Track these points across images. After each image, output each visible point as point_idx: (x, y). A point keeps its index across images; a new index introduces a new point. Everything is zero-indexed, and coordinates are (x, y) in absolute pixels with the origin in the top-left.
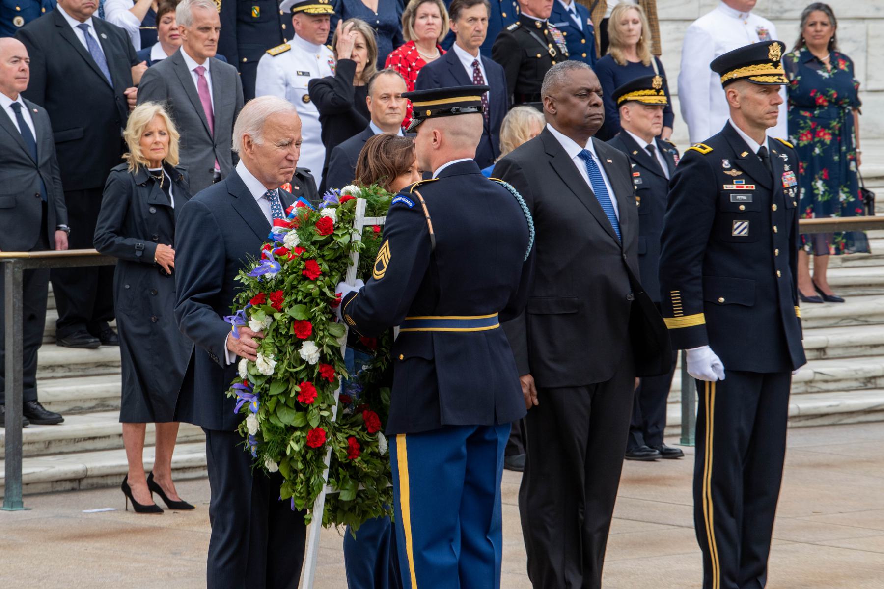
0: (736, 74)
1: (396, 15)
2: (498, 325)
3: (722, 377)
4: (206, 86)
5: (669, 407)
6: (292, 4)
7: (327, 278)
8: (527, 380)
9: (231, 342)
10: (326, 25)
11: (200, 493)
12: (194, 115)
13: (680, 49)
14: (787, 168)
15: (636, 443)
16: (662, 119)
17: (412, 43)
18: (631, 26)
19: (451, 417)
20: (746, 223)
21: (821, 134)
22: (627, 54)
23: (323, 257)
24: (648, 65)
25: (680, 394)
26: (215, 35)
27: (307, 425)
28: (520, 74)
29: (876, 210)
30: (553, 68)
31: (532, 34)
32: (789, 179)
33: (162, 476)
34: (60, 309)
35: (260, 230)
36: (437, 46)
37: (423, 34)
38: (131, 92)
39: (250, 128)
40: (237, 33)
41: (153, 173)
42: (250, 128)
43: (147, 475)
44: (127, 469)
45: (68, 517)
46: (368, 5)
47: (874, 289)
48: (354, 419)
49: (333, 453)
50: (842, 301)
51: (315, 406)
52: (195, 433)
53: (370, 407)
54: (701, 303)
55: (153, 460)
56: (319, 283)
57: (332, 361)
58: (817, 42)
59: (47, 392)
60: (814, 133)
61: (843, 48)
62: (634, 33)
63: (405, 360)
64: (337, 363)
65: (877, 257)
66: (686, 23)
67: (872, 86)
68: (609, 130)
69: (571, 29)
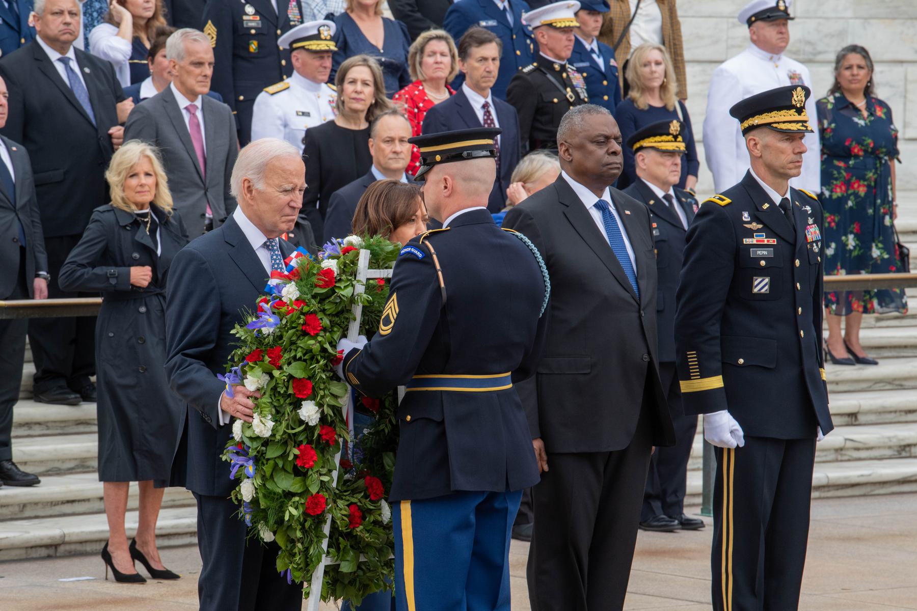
0: (757, 120)
1: (403, 53)
2: (511, 385)
3: (742, 444)
4: (198, 125)
5: (689, 475)
6: (291, 40)
7: (328, 334)
8: (537, 444)
9: (225, 402)
10: (328, 63)
11: (189, 564)
12: (185, 155)
13: (706, 92)
14: (810, 221)
15: (654, 513)
16: (680, 166)
17: (419, 83)
18: (654, 67)
19: (462, 482)
20: (767, 280)
21: (856, 186)
22: (649, 98)
23: (324, 311)
24: (671, 109)
25: (701, 461)
26: (209, 71)
27: (307, 491)
28: (535, 119)
29: (911, 266)
30: (570, 111)
31: (549, 76)
32: (813, 232)
33: (145, 543)
34: (37, 361)
35: (257, 279)
36: (446, 86)
37: (430, 73)
38: (116, 131)
39: (250, 172)
40: (234, 69)
41: (138, 215)
42: (250, 172)
43: (130, 542)
44: (107, 535)
45: (42, 586)
46: (373, 42)
47: (910, 351)
48: (355, 485)
49: (333, 522)
50: (876, 363)
51: (315, 470)
52: (182, 497)
53: (373, 472)
54: (719, 364)
55: (136, 525)
56: (320, 339)
57: (333, 422)
58: (853, 86)
59: (24, 453)
60: (848, 184)
61: (881, 93)
62: (656, 75)
63: (412, 421)
64: (339, 424)
65: (913, 317)
66: (713, 65)
67: (910, 133)
68: (627, 179)
69: (592, 71)
